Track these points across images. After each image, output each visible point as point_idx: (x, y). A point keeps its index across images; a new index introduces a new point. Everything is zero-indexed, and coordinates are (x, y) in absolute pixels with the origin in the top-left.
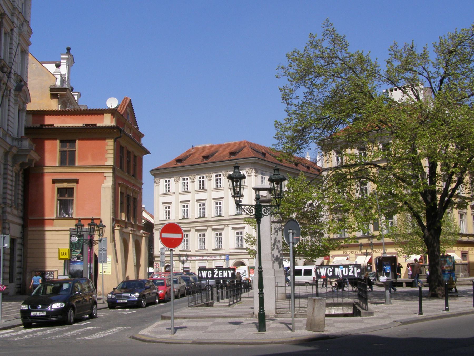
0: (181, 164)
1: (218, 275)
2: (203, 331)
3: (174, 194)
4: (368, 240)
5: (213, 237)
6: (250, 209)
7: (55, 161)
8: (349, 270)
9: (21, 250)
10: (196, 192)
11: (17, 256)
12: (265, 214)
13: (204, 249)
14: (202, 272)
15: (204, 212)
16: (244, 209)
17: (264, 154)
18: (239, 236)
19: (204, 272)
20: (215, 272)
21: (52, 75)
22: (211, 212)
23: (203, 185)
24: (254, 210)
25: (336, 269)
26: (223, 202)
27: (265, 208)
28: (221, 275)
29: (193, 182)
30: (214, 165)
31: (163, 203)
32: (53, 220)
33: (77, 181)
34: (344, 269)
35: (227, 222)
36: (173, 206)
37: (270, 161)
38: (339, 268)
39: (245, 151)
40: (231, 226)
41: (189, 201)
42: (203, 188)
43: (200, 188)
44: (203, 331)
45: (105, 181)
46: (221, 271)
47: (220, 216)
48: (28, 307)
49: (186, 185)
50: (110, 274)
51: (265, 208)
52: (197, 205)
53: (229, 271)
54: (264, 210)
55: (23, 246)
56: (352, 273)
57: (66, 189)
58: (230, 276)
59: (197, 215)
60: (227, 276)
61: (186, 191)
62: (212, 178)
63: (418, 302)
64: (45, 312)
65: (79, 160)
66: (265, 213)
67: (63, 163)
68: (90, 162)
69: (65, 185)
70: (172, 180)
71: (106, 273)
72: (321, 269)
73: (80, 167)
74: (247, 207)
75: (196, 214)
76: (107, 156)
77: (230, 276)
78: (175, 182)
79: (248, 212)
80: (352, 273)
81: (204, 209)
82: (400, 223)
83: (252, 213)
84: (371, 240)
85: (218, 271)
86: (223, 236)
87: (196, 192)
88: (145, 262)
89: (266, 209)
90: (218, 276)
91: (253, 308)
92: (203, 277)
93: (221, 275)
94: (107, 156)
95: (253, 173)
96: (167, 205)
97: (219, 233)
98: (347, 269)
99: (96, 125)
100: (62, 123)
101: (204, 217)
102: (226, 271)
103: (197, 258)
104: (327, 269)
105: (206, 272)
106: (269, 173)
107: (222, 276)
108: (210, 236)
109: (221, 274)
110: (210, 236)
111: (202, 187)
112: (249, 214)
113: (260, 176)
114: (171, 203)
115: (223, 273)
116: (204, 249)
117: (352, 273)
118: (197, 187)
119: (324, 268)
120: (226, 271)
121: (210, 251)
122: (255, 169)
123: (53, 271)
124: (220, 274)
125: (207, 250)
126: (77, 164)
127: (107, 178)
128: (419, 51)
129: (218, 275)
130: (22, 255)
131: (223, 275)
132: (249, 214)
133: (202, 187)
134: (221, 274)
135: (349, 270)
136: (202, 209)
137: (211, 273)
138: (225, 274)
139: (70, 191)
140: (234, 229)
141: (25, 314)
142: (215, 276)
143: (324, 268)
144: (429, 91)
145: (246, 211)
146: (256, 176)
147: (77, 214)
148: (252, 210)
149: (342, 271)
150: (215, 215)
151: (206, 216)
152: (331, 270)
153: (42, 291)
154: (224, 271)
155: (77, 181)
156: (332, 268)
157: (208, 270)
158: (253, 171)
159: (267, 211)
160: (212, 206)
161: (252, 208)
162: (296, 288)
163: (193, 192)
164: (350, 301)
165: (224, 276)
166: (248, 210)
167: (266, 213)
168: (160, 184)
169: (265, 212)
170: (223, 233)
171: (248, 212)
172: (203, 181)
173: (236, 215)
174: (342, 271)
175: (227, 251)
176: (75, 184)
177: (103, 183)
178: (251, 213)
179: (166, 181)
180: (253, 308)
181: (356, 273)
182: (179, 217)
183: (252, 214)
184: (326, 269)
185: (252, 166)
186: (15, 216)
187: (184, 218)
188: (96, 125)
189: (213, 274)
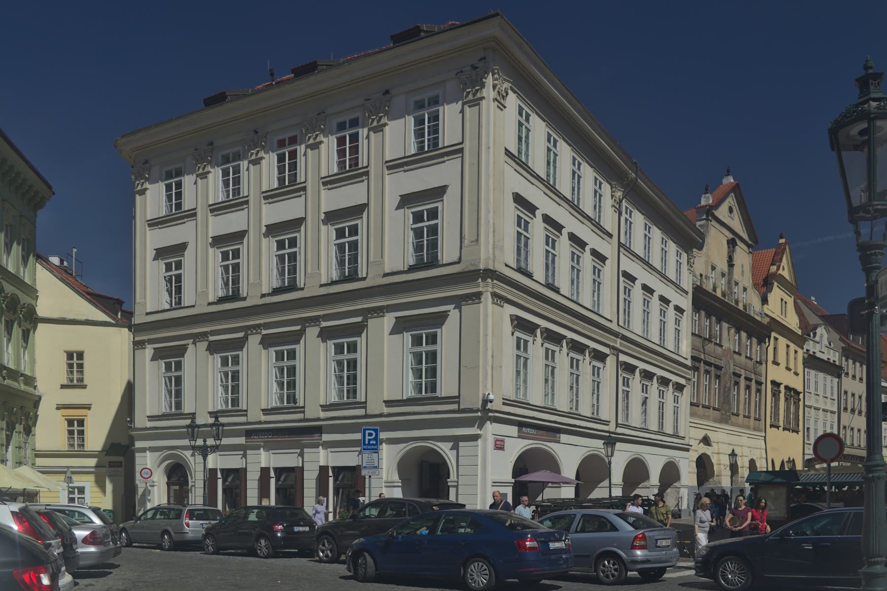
3: (192, 214)
40: (389, 320)
49: (232, 181)
59: (216, 289)
150: (335, 276)
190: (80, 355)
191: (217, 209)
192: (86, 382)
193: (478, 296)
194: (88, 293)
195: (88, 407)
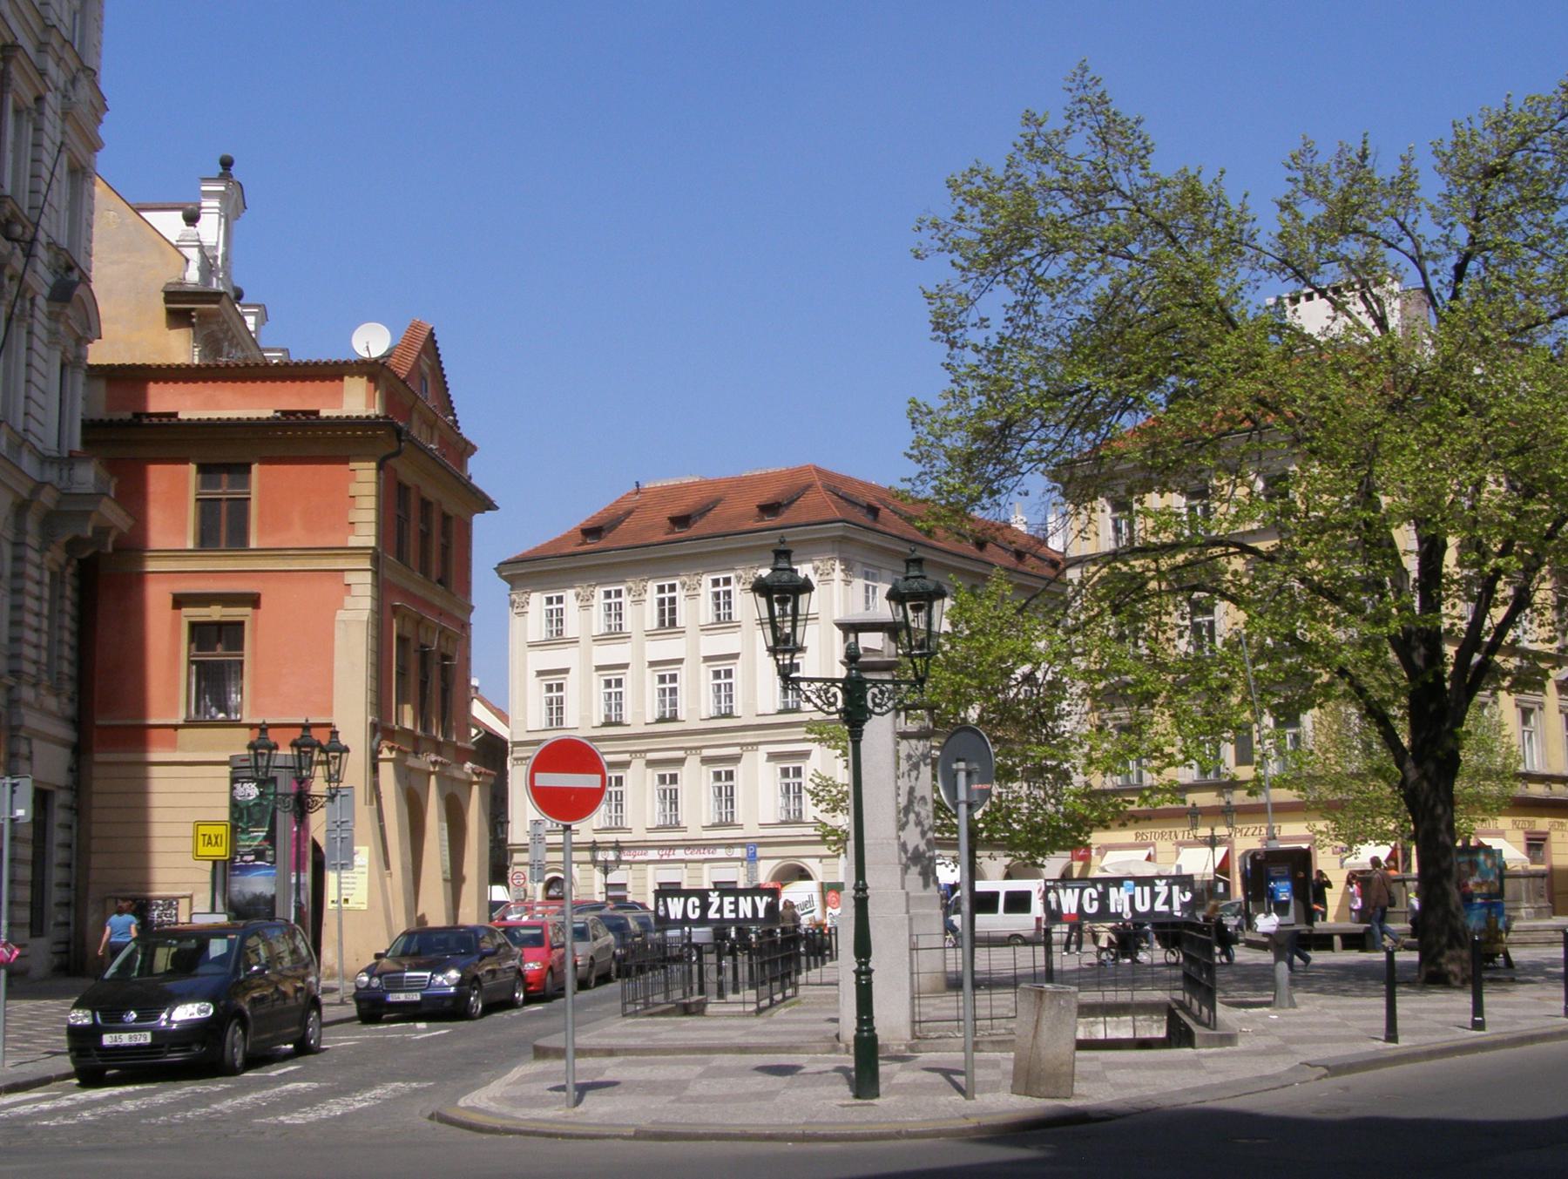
0: (600, 544)
1: (720, 909)
2: (672, 1098)
3: (575, 641)
4: (1218, 796)
5: (704, 786)
6: (827, 692)
7: (183, 532)
8: (1154, 896)
9: (70, 827)
10: (650, 634)
11: (55, 848)
12: (877, 710)
13: (676, 826)
14: (669, 900)
15: (674, 704)
16: (809, 693)
17: (873, 511)
18: (792, 780)
19: (676, 899)
20: (710, 900)
21: (172, 249)
22: (696, 703)
23: (673, 611)
24: (840, 695)
25: (1113, 891)
26: (738, 668)
27: (876, 690)
28: (731, 911)
29: (638, 602)
30: (709, 546)
31: (540, 673)
32: (176, 727)
33: (253, 600)
34: (1138, 889)
35: (750, 737)
36: (571, 682)
37: (895, 532)
38: (1122, 889)
39: (810, 498)
40: (764, 750)
41: (626, 666)
42: (673, 623)
43: (662, 623)
44: (672, 1098)
45: (347, 599)
46: (732, 899)
47: (729, 715)
48: (94, 1017)
49: (614, 611)
50: (364, 907)
51: (876, 690)
52: (651, 678)
53: (757, 899)
54: (874, 696)
55: (77, 813)
56: (1164, 904)
57: (220, 626)
58: (761, 914)
59: (652, 711)
60: (749, 915)
61: (615, 634)
62: (701, 591)
63: (1382, 1001)
64: (148, 1034)
65: (261, 531)
66: (875, 705)
67: (207, 539)
68: (296, 536)
69: (216, 613)
70: (569, 595)
71: (349, 905)
72: (1061, 892)
73: (264, 552)
74: (818, 685)
75: (648, 709)
76: (354, 516)
77: (761, 914)
78: (579, 603)
79: (819, 703)
80: (1165, 903)
81: (673, 691)
82: (1322, 739)
83: (834, 704)
84: (1227, 796)
85: (721, 896)
86: (739, 782)
87: (650, 634)
88: (480, 868)
89: (882, 692)
90: (722, 915)
91: (836, 1020)
92: (672, 917)
93: (731, 911)
94: (354, 516)
95: (838, 574)
96: (554, 679)
97: (724, 771)
98: (1147, 889)
99: (316, 413)
100: (206, 407)
101: (674, 718)
102: (749, 899)
103: (653, 855)
104: (1082, 890)
105: (682, 899)
106: (889, 573)
107: (733, 916)
108: (696, 782)
109: (732, 907)
110: (696, 782)
111: (668, 620)
112: (825, 707)
113: (859, 583)
114: (566, 671)
115: (736, 903)
116: (676, 826)
117: (1164, 904)
118: (652, 620)
119: (1073, 889)
120: (749, 899)
121: (694, 832)
122: (843, 560)
123: (176, 898)
124: (727, 907)
125: (685, 829)
126: (253, 544)
127: (355, 590)
128: (1385, 169)
129: (720, 909)
130: (74, 846)
131: (736, 910)
132: (825, 707)
133: (668, 620)
134: (732, 907)
135: (1154, 896)
136: (669, 693)
137: (697, 903)
138: (745, 906)
139: (231, 633)
140: (773, 757)
141: (82, 1041)
142: (712, 914)
143: (1073, 889)
144: (1419, 303)
145: (813, 697)
146: (847, 583)
147: (255, 709)
148: (835, 695)
149: (1132, 898)
150: (713, 712)
151: (681, 715)
152: (1095, 895)
153: (138, 964)
154: (741, 899)
155: (253, 600)
156: (1100, 887)
157: (687, 894)
158: (837, 565)
159: (882, 699)
160: (703, 683)
161: (834, 689)
162: (980, 953)
163: (637, 636)
164: (1159, 995)
165: (741, 916)
166: (819, 697)
167: (880, 706)
168: (529, 608)
169: (877, 701)
170: (739, 770)
171: (819, 703)
172: (672, 601)
173: (780, 712)
174: (1132, 898)
175: (751, 830)
176: (248, 610)
177: (342, 608)
178: (830, 704)
179: (550, 601)
180: (836, 1020)
181: (1176, 906)
182: (591, 719)
183: (833, 709)
184: (1077, 891)
185: (833, 551)
186: (51, 714)
187: (608, 723)
188: (316, 413)
189: (705, 906)
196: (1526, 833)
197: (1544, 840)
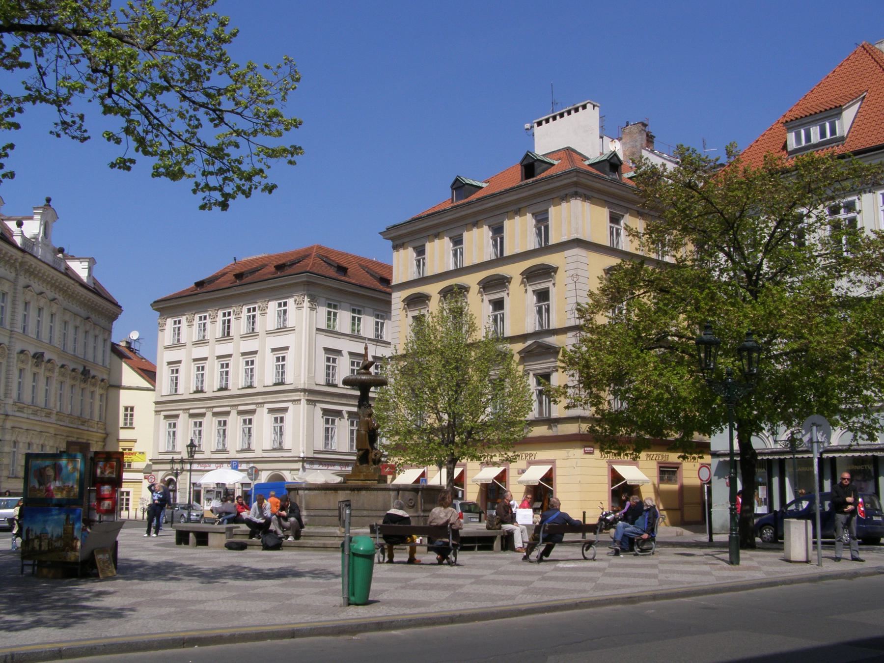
0: (204, 290)
2: (493, 571)
4: (549, 429)
5: (213, 428)
10: (218, 341)
13: (224, 451)
15: (227, 380)
22: (238, 381)
23: (229, 327)
26: (257, 359)
29: (190, 326)
30: (264, 286)
31: (274, 350)
35: (260, 399)
36: (182, 368)
39: (309, 262)
41: (206, 359)
43: (224, 336)
44: (493, 571)
62: (242, 315)
70: (183, 319)
75: (240, 382)
78: (296, 306)
84: (554, 429)
86: (254, 426)
87: (218, 341)
95: (306, 304)
97: (278, 414)
101: (226, 389)
110: (263, 421)
111: (227, 334)
113: (323, 311)
114: (287, 348)
116: (224, 451)
118: (219, 334)
122: (310, 296)
125: (253, 451)
133: (227, 334)
140: (271, 411)
144: (640, 131)
146: (312, 309)
151: (230, 387)
158: (306, 299)
160: (216, 369)
163: (212, 341)
168: (268, 311)
170: (255, 418)
172: (229, 321)
175: (258, 454)
179: (280, 305)
182: (190, 389)
185: (304, 290)
190: (132, 409)
191: (195, 344)
192: (134, 425)
193: (300, 400)
194: (139, 369)
195: (135, 441)
196: (659, 463)
197: (677, 468)
